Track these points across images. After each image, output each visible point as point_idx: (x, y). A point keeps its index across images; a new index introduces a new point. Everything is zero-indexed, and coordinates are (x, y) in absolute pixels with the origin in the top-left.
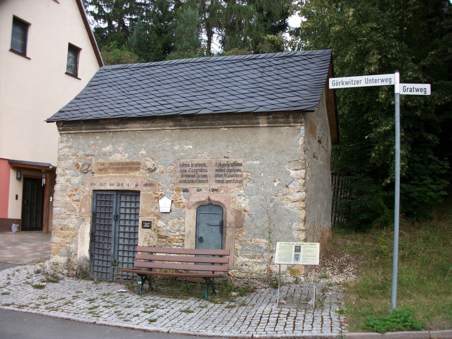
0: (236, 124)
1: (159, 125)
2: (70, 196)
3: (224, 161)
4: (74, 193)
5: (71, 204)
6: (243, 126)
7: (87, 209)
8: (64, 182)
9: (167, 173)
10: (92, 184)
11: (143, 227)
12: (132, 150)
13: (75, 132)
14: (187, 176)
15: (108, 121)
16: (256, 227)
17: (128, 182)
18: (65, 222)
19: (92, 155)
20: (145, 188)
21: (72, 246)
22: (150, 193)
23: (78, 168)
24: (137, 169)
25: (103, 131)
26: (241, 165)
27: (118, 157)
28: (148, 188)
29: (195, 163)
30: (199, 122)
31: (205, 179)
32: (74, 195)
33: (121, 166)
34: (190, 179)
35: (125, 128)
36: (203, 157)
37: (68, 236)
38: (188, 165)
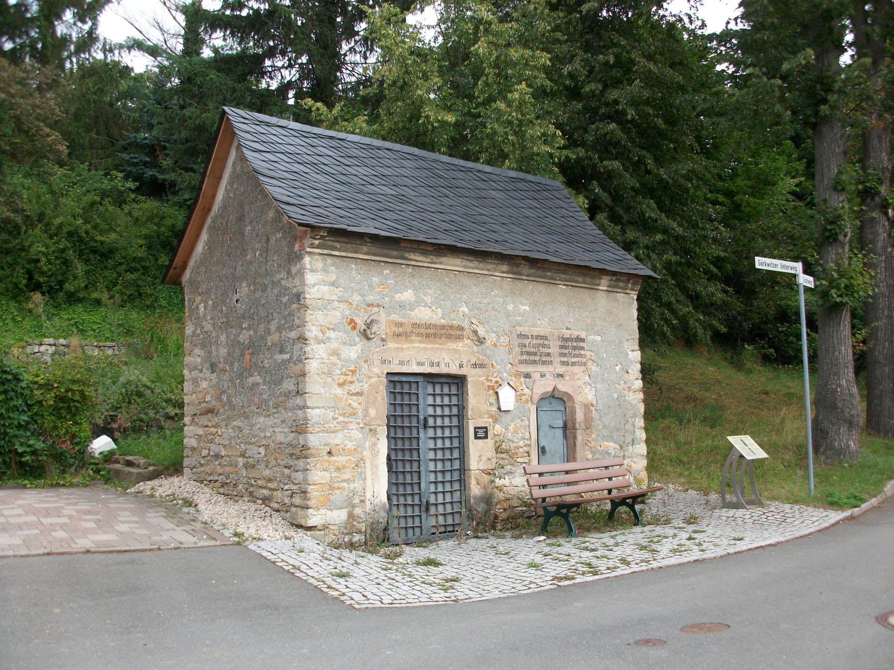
0: (577, 282)
1: (489, 267)
2: (340, 385)
3: (567, 334)
4: (349, 378)
5: (347, 400)
6: (583, 285)
7: (379, 408)
8: (325, 356)
9: (501, 348)
10: (384, 362)
11: (476, 437)
12: (448, 303)
13: (343, 254)
14: (528, 353)
15: (416, 246)
16: (605, 427)
17: (446, 359)
18: (336, 439)
19: (378, 306)
20: (475, 371)
21: (357, 485)
22: (481, 379)
23: (354, 328)
24: (459, 338)
25: (398, 261)
26: (583, 340)
27: (425, 314)
28: (478, 370)
29: (535, 334)
30: (539, 273)
31: (548, 359)
32: (351, 382)
33: (432, 331)
34: (532, 358)
35: (435, 263)
36: (543, 327)
37: (344, 467)
38: (525, 336)
